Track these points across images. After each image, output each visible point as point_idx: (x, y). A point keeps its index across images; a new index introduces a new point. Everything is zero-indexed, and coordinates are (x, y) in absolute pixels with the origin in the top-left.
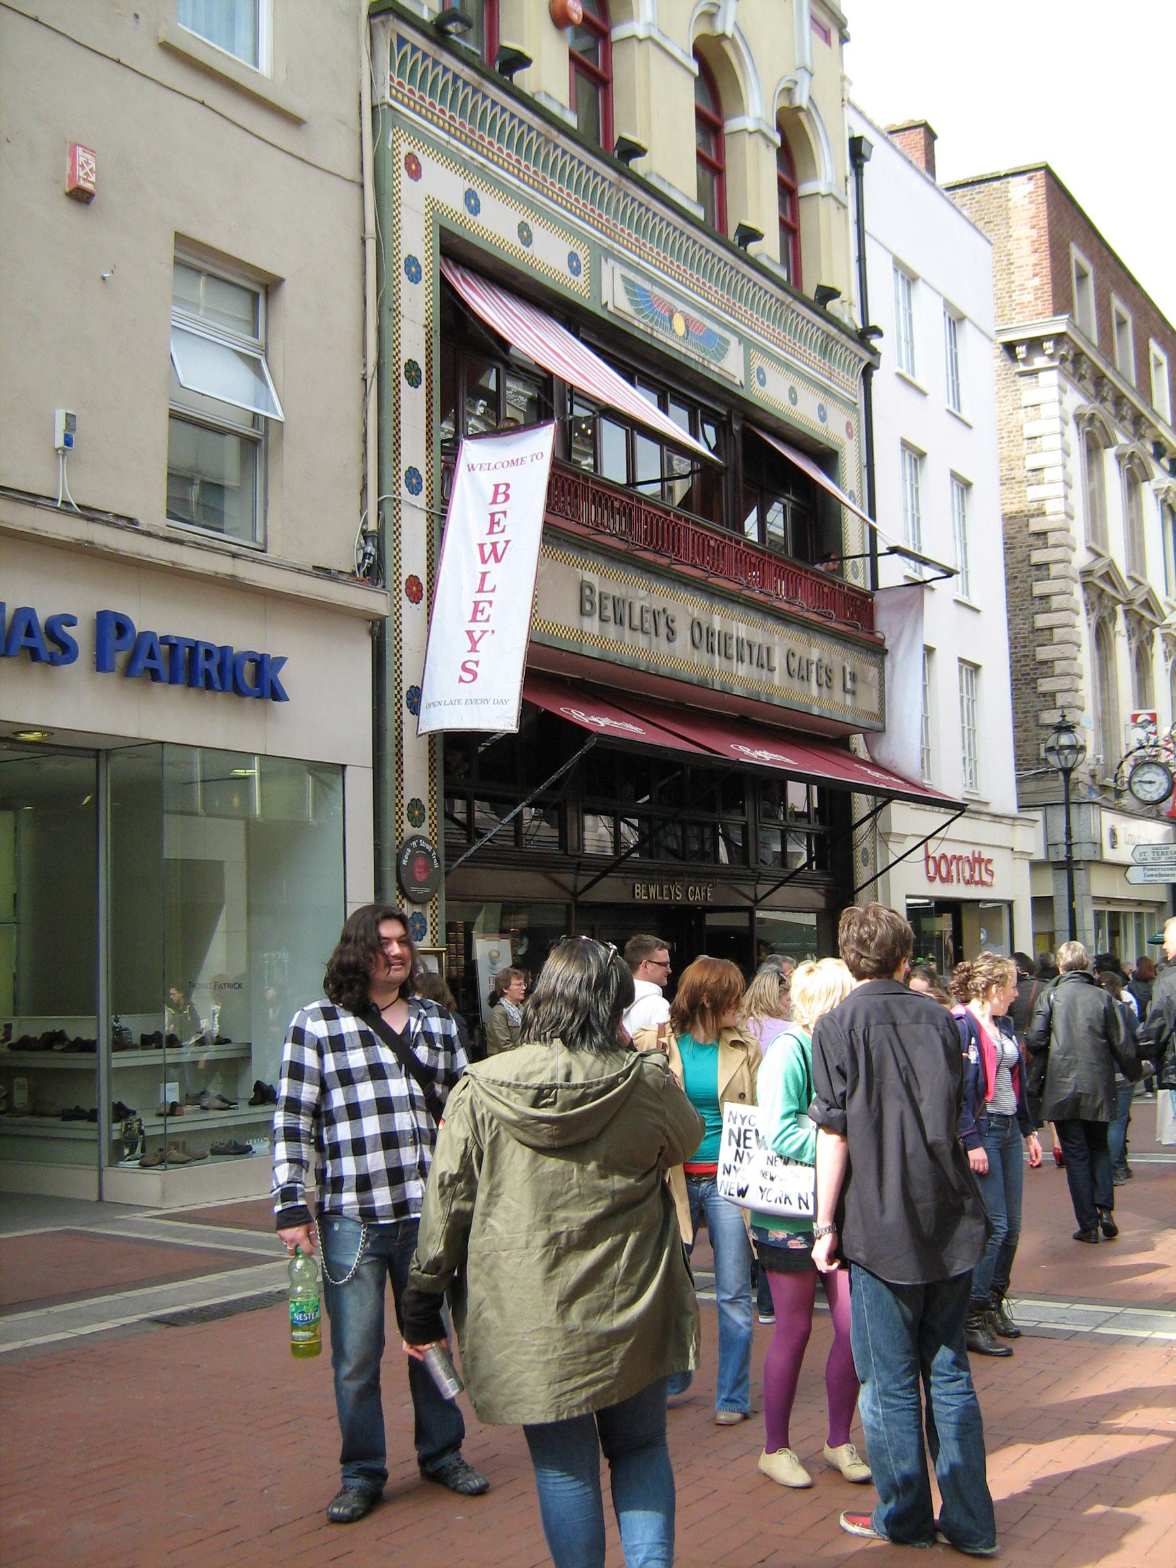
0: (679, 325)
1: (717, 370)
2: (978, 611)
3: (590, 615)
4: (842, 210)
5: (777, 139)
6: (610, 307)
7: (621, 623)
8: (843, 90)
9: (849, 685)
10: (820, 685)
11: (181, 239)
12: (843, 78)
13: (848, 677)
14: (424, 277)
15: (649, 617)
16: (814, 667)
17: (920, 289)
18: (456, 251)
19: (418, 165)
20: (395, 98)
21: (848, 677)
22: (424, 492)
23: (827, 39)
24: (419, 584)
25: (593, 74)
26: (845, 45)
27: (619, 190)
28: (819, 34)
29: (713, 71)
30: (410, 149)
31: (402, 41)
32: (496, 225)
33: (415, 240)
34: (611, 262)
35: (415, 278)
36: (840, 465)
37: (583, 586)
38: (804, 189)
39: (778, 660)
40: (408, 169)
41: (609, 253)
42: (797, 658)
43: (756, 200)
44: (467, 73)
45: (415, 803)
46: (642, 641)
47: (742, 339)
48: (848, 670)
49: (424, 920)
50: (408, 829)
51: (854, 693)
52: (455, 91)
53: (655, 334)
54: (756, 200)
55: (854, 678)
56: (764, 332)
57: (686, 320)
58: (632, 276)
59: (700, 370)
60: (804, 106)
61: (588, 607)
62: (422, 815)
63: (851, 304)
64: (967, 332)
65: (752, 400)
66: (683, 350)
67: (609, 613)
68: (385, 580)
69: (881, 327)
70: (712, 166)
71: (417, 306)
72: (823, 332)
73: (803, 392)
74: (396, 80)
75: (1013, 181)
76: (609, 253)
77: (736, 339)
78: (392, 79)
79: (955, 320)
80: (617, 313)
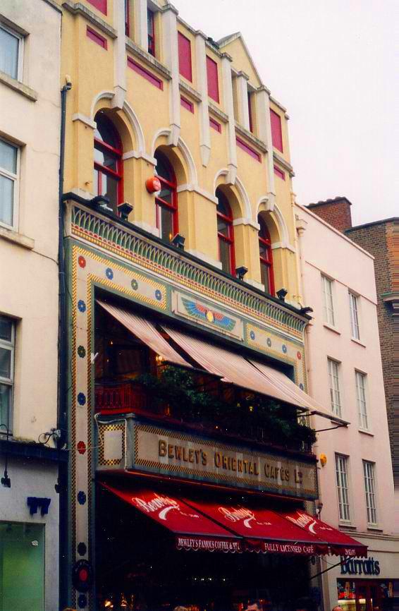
0: (210, 317)
1: (230, 335)
2: (372, 436)
3: (163, 455)
4: (292, 254)
5: (258, 227)
6: (176, 313)
7: (180, 459)
8: (292, 199)
9: (298, 479)
10: (282, 480)
11: (363, 460)
12: (292, 194)
13: (297, 474)
14: (87, 309)
15: (193, 454)
16: (279, 471)
17: (336, 285)
18: (102, 294)
19: (84, 261)
20: (74, 233)
21: (297, 474)
22: (87, 503)
23: (283, 178)
24: (84, 350)
25: (169, 209)
26: (293, 178)
27: (179, 260)
28: (279, 176)
29: (226, 201)
30: (81, 254)
31: (77, 209)
32: (121, 284)
33: (82, 292)
34: (176, 292)
35: (82, 310)
36: (295, 374)
37: (161, 442)
38: (274, 246)
39: (260, 470)
40: (80, 263)
41: (175, 289)
42: (270, 468)
43: (249, 254)
44: (107, 219)
45: (82, 545)
46: (190, 466)
47: (242, 319)
48: (297, 471)
49: (86, 598)
50: (79, 557)
51: (301, 482)
52: (102, 227)
53: (198, 322)
54: (249, 254)
55: (301, 475)
56: (253, 315)
57: (214, 315)
58: (186, 297)
59: (221, 336)
60: (272, 210)
61: (163, 452)
62: (84, 307)
63: (298, 297)
64: (362, 303)
65: (247, 347)
66: (213, 328)
67: (173, 453)
68: (67, 444)
69: (311, 307)
70: (227, 241)
71: (83, 322)
72: (284, 312)
73: (274, 340)
74: (74, 225)
75: (388, 224)
76: (175, 289)
77: (239, 320)
78: (72, 225)
79: (355, 296)
80: (179, 314)
